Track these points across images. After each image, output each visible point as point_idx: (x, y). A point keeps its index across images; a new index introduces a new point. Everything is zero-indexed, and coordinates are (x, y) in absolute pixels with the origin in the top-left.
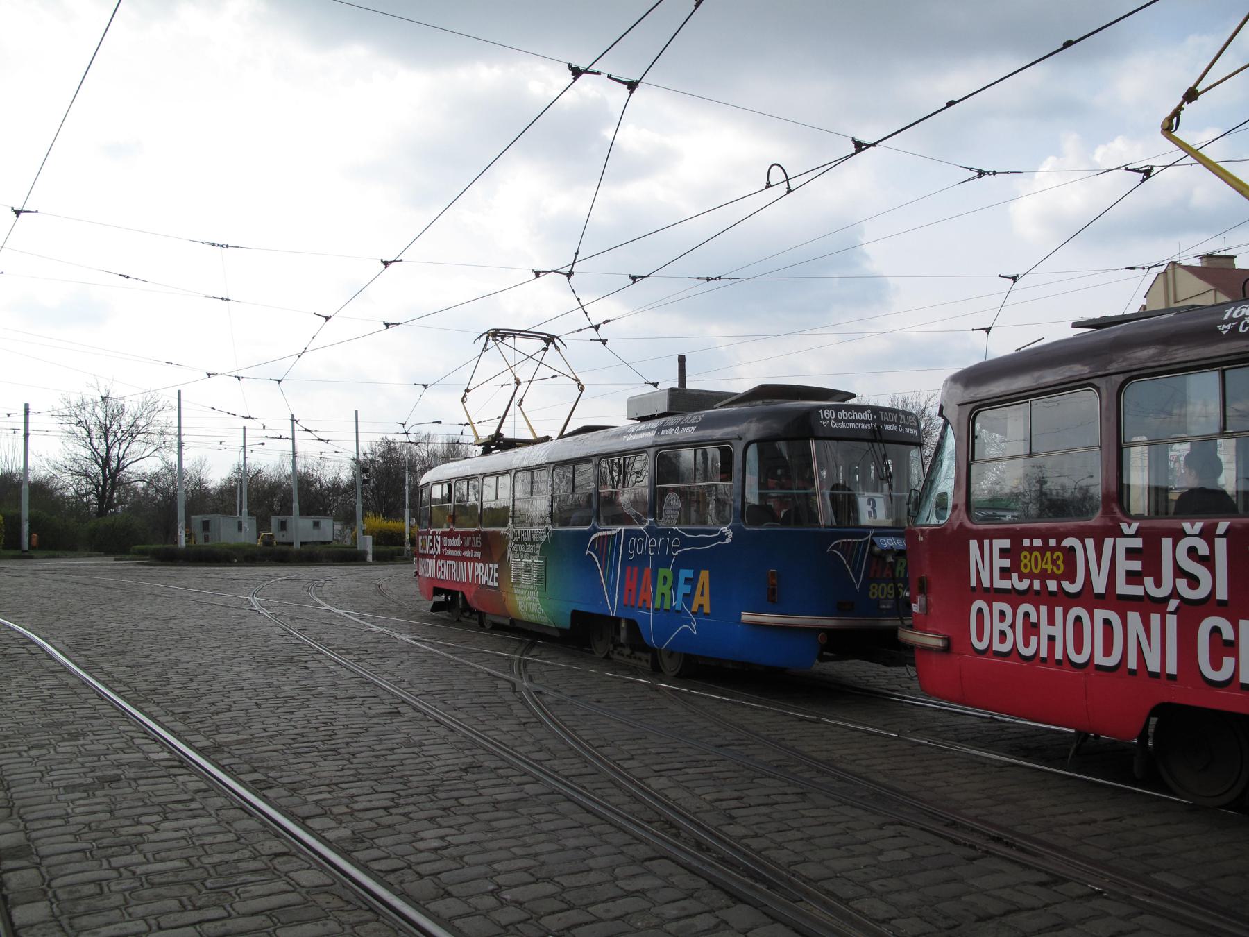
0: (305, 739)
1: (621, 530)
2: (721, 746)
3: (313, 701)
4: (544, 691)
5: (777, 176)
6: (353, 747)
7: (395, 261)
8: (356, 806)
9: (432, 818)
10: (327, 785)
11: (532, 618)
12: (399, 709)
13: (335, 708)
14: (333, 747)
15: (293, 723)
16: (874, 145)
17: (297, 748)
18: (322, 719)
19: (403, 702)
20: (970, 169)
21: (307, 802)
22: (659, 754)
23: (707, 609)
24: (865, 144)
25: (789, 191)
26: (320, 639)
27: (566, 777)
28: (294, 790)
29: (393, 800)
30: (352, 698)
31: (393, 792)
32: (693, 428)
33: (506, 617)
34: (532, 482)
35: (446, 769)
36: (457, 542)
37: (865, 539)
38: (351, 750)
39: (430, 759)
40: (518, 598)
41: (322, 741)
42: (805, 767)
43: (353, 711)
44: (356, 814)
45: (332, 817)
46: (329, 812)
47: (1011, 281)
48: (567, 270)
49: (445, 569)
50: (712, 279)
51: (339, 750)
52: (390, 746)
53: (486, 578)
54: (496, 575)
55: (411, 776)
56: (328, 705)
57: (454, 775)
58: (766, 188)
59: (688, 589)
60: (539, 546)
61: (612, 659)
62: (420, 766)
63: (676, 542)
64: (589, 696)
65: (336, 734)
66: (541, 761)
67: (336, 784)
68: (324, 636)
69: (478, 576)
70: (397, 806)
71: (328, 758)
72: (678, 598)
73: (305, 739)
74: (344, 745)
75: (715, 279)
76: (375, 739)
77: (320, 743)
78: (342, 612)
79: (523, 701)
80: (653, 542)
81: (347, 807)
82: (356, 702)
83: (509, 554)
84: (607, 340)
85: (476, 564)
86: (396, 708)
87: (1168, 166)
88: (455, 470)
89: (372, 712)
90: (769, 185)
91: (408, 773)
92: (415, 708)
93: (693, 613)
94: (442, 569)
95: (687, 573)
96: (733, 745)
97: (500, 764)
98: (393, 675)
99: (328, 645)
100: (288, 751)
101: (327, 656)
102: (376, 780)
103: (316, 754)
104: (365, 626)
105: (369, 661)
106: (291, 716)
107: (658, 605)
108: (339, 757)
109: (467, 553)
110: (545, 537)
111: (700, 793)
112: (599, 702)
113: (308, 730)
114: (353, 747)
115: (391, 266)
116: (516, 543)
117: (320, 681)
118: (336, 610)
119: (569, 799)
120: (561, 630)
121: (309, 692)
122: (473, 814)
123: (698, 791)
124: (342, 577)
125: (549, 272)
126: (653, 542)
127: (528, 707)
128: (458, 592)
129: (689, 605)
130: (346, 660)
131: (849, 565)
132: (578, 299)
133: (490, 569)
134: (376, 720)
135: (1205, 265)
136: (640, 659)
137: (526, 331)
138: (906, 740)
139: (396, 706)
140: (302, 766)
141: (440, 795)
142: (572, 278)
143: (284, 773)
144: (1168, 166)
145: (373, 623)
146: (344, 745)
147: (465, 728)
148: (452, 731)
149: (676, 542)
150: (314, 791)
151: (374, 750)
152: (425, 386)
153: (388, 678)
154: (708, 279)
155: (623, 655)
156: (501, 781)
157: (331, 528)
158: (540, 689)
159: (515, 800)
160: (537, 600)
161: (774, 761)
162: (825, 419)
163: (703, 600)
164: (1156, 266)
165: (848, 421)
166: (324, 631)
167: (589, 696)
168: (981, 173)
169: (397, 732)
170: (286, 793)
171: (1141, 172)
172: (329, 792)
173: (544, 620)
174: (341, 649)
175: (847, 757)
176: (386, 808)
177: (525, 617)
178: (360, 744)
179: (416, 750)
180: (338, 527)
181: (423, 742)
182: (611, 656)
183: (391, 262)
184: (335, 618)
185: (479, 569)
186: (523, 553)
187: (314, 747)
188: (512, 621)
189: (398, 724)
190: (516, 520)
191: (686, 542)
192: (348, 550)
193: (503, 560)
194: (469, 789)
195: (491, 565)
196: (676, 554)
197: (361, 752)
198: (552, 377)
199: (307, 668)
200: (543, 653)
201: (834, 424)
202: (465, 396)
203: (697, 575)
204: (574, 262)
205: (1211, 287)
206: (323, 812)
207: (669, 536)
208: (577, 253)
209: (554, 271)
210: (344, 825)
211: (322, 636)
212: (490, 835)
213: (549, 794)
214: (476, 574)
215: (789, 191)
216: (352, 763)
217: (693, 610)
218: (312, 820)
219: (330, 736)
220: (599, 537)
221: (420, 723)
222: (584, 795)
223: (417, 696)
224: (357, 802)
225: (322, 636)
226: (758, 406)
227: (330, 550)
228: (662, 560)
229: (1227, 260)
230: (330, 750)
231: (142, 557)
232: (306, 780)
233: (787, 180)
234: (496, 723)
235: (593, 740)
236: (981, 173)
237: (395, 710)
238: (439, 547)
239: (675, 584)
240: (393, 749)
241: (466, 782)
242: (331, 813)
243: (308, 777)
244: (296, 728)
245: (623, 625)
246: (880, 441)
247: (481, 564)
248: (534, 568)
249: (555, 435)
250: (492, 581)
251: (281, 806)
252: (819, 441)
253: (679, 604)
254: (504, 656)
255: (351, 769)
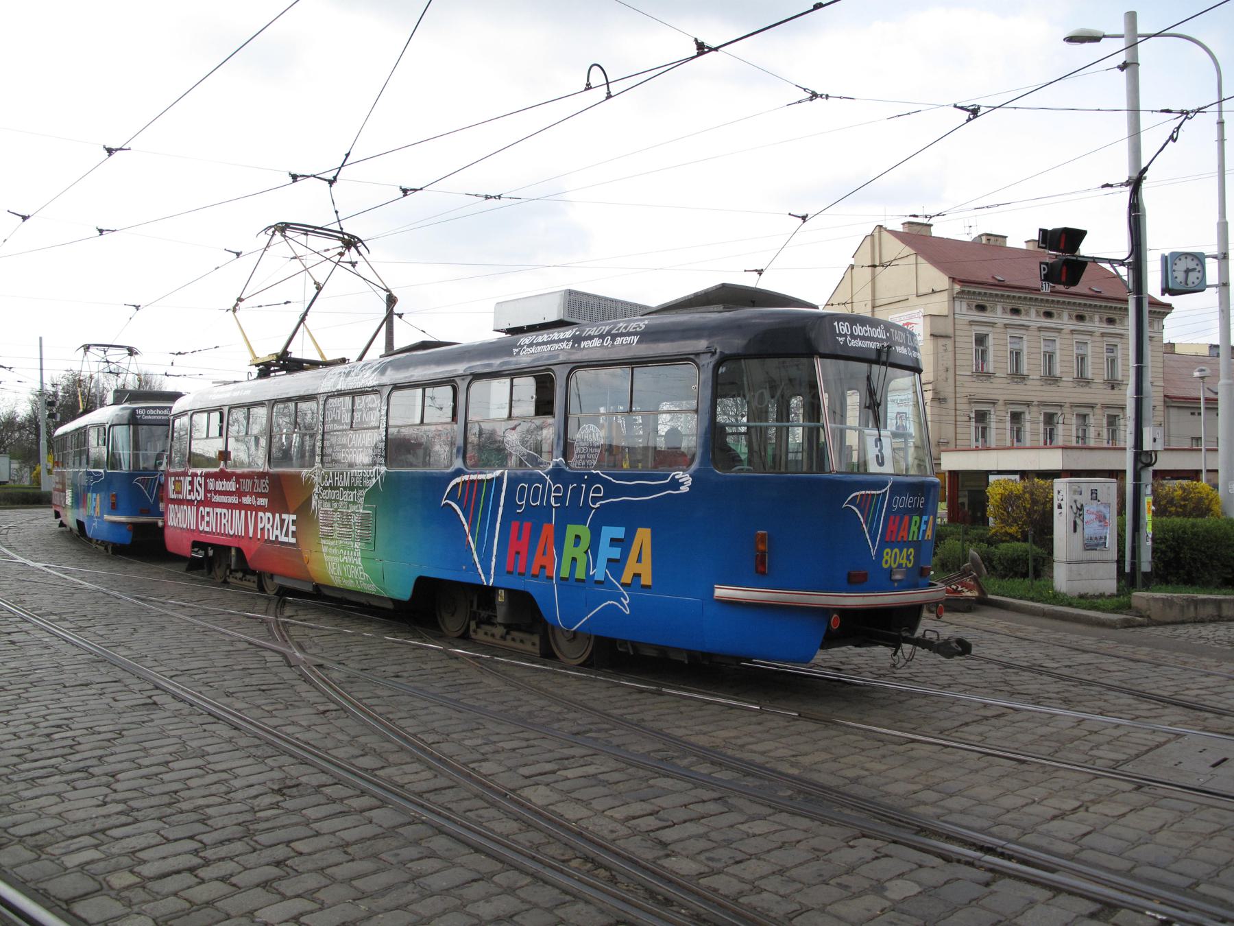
0: (35, 755)
1: (503, 474)
2: (578, 734)
3: (33, 692)
4: (327, 663)
5: (597, 78)
6: (109, 764)
7: (121, 149)
8: (147, 870)
9: (266, 882)
10: (91, 834)
11: (350, 584)
12: (154, 698)
13: (66, 702)
14: (81, 764)
15: (12, 730)
16: (716, 49)
17: (28, 770)
18: (52, 719)
19: (157, 688)
20: (805, 90)
21: (66, 869)
22: (514, 750)
23: (646, 580)
24: (708, 47)
25: (609, 96)
26: (21, 602)
27: (420, 795)
28: (40, 848)
29: (196, 852)
30: (86, 685)
31: (191, 838)
32: (636, 339)
33: (309, 580)
34: (353, 411)
35: (253, 791)
36: (231, 486)
37: (884, 491)
38: (109, 768)
39: (224, 776)
40: (327, 558)
41: (62, 756)
42: (695, 759)
43: (93, 704)
44: (150, 885)
45: (113, 893)
46: (105, 885)
47: (800, 221)
48: (330, 176)
49: (212, 519)
50: (491, 197)
51: (91, 770)
52: (161, 759)
53: (278, 532)
54: (293, 528)
55: (208, 806)
56: (57, 696)
57: (267, 800)
58: (586, 89)
59: (616, 553)
60: (363, 493)
61: (228, 583)
62: (214, 789)
63: (597, 490)
64: (383, 669)
65: (79, 744)
66: (373, 770)
67: (103, 831)
68: (26, 598)
69: (263, 529)
70: (207, 863)
71: (78, 784)
72: (598, 565)
73: (35, 755)
74: (95, 762)
75: (495, 197)
76: (137, 747)
77: (60, 759)
78: (39, 565)
79: (307, 680)
80: (558, 490)
81: (132, 872)
82: (93, 692)
83: (314, 502)
84: (356, 262)
85: (261, 514)
86: (150, 697)
87: (995, 108)
88: (228, 395)
89: (121, 705)
90: (589, 87)
91: (201, 802)
92: (174, 696)
93: (623, 585)
94: (207, 519)
95: (610, 532)
96: (591, 731)
97: (324, 779)
98: (129, 648)
99: (33, 609)
100: (15, 777)
101: (36, 625)
102: (160, 819)
103: (57, 778)
104: (73, 583)
105: (92, 629)
106: (9, 718)
107: (565, 573)
108: (93, 781)
109: (247, 500)
110: (374, 481)
111: (601, 808)
112: (397, 677)
113: (36, 739)
114: (109, 764)
115: (116, 155)
116: (325, 488)
117: (35, 660)
118: (32, 564)
119: (441, 831)
120: (395, 601)
121: (24, 679)
122: (322, 869)
123: (596, 805)
124: (28, 522)
125: (308, 177)
126: (558, 490)
127: (317, 688)
128: (229, 548)
129: (618, 574)
130: (62, 629)
131: (866, 523)
132: (336, 212)
133: (282, 521)
134: (128, 718)
135: (907, 230)
136: (249, 581)
137: (322, 228)
138: (842, 725)
139: (149, 693)
140: (43, 801)
141: (263, 838)
142: (334, 185)
143: (17, 818)
144: (995, 108)
145: (81, 579)
146: (95, 762)
147: (205, 701)
148: (236, 728)
149: (597, 490)
150: (73, 847)
151: (140, 767)
152: (137, 307)
153: (124, 653)
154: (487, 197)
155: (236, 578)
156: (337, 807)
157: (7, 467)
158: (320, 661)
159: (369, 839)
160: (359, 562)
161: (655, 751)
162: (840, 335)
163: (640, 565)
164: (938, 215)
165: (863, 338)
166: (23, 591)
167: (383, 669)
168: (814, 95)
169: (163, 734)
170: (30, 855)
171: (968, 110)
172: (96, 847)
173: (371, 588)
174: (52, 614)
175: (733, 741)
176: (191, 870)
177: (337, 582)
178: (119, 757)
179: (200, 762)
180: (15, 465)
181: (206, 749)
182: (228, 580)
183: (117, 150)
184: (33, 573)
185: (265, 520)
186: (338, 501)
187: (53, 766)
188: (317, 587)
189: (163, 722)
190: (326, 459)
191: (611, 490)
192: (26, 491)
193: (304, 511)
194: (296, 824)
195: (284, 516)
196: (597, 505)
197: (124, 771)
198: (286, 303)
199: (13, 643)
200: (300, 613)
201: (850, 342)
202: (237, 305)
203: (630, 535)
204: (342, 166)
205: (913, 252)
206: (97, 886)
207: (585, 481)
208: (347, 155)
209: (314, 176)
210: (136, 909)
211: (22, 597)
212: (363, 906)
213: (410, 823)
214: (260, 526)
215: (609, 96)
216: (115, 791)
217: (623, 581)
218: (83, 903)
219: (71, 747)
220: (464, 482)
221: (189, 718)
222: (455, 822)
223: (171, 677)
224: (145, 862)
225: (22, 597)
226: (713, 315)
227: (7, 491)
228: (574, 513)
229: (925, 228)
230: (78, 771)
231: (636, 877)
232: (55, 828)
233: (608, 83)
234: (287, 713)
235: (423, 732)
236: (814, 95)
237: (149, 701)
238: (202, 492)
239: (594, 546)
240: (167, 763)
241: (289, 812)
242: (111, 888)
243: (57, 822)
244: (19, 738)
245: (233, 553)
246: (884, 364)
247: (269, 515)
248: (355, 519)
249: (353, 356)
250: (287, 535)
251: (25, 882)
252: (825, 360)
253: (600, 572)
254: (256, 618)
255: (118, 802)
